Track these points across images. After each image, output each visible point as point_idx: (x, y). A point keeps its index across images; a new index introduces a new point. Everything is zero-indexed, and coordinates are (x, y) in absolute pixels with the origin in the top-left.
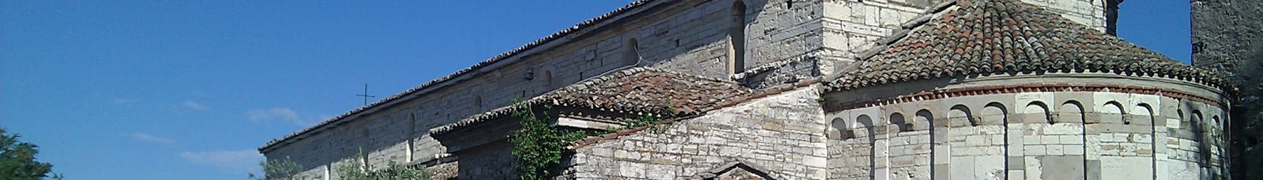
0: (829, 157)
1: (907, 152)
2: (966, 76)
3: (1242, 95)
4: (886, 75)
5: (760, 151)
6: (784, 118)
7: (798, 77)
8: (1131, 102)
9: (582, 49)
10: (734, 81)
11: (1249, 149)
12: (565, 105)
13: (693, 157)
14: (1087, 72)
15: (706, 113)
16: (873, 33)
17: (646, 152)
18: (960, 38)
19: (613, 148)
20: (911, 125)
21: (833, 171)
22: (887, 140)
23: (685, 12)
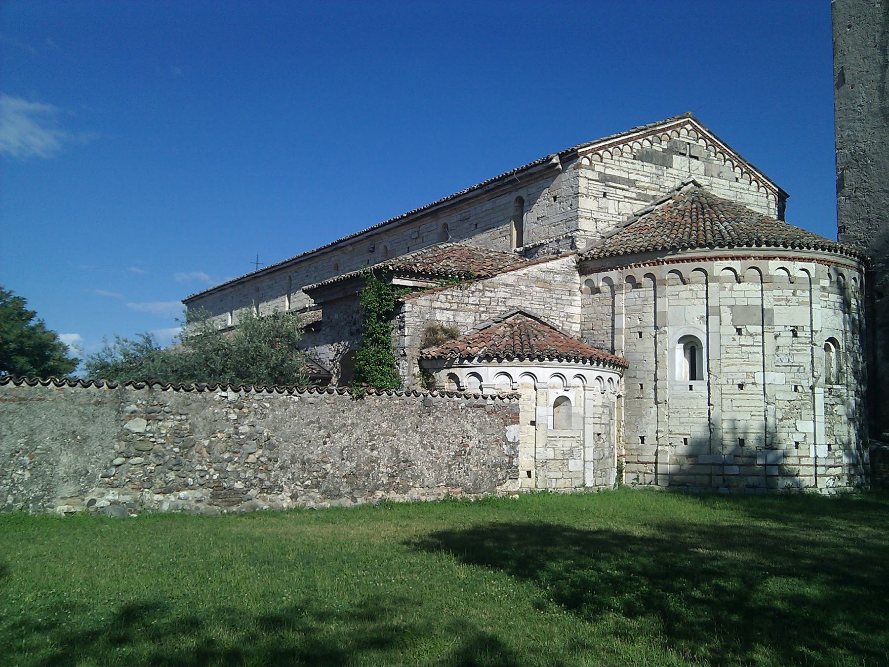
0: (583, 307)
1: (637, 303)
2: (679, 249)
4: (622, 249)
5: (534, 302)
6: (551, 279)
7: (561, 250)
8: (795, 268)
9: (409, 231)
11: (878, 301)
12: (397, 270)
13: (487, 306)
14: (764, 246)
15: (496, 275)
16: (614, 219)
19: (431, 300)
20: (640, 284)
23: (481, 205)
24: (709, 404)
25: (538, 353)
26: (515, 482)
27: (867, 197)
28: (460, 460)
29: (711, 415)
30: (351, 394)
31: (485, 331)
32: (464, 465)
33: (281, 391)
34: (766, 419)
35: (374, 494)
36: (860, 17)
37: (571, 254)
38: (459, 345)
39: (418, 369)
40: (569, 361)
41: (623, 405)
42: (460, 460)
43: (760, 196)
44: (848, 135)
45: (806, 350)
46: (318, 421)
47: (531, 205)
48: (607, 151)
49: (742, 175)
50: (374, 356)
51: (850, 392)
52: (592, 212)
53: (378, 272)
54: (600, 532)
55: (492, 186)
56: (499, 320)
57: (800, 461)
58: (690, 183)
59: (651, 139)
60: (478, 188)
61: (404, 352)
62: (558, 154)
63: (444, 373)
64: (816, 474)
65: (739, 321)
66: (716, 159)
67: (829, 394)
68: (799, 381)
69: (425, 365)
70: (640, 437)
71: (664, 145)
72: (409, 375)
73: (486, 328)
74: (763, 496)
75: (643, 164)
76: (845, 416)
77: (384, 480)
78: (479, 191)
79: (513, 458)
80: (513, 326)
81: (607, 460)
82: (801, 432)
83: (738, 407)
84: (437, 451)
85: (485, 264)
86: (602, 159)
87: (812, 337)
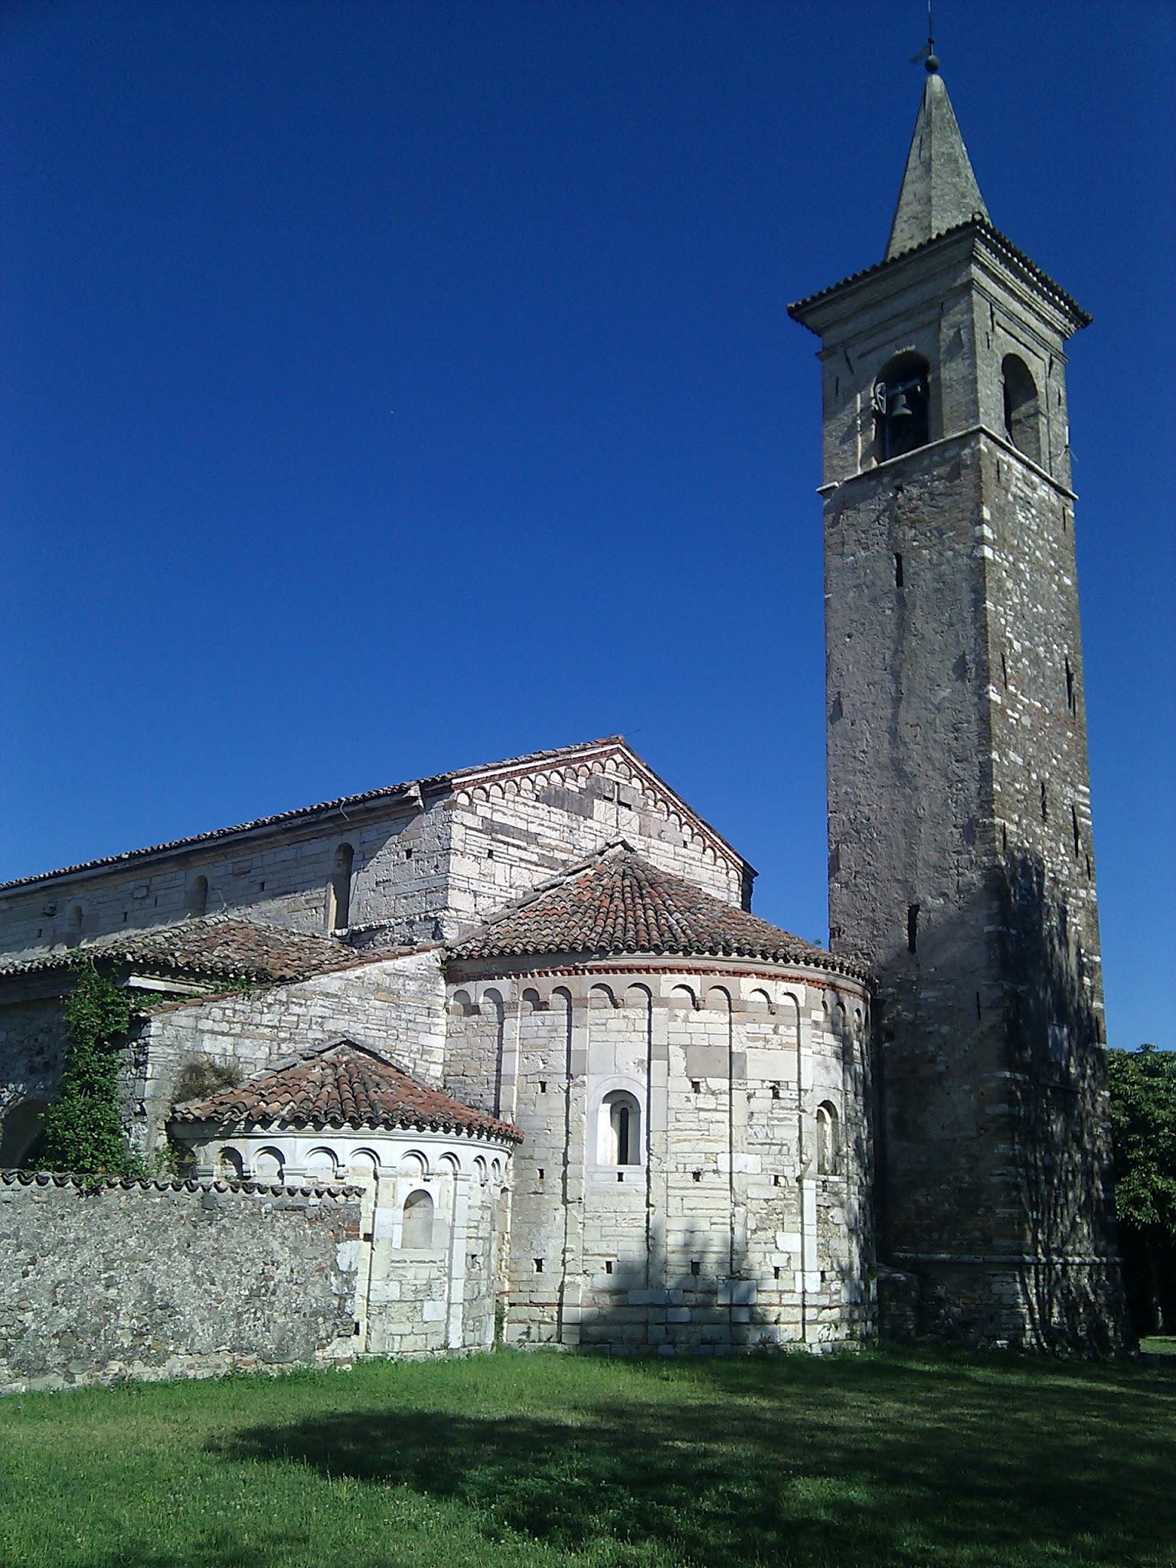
0: (449, 1035)
1: (540, 1034)
2: (609, 952)
3: (880, 988)
4: (520, 945)
5: (370, 1026)
6: (400, 987)
7: (415, 939)
8: (778, 990)
9: (129, 884)
10: (334, 938)
11: (887, 1045)
12: (141, 961)
13: (292, 1030)
14: (734, 955)
15: (310, 978)
16: (503, 894)
17: (236, 1023)
18: (600, 907)
19: (196, 1017)
20: (546, 1003)
21: (451, 1052)
22: (519, 1019)
23: (273, 850)
24: (648, 1205)
25: (385, 1115)
26: (346, 1343)
27: (872, 887)
28: (258, 1304)
29: (651, 1222)
30: (78, 1185)
31: (286, 1074)
32: (263, 1313)
33: (28, 1181)
34: (732, 1229)
35: (106, 1366)
36: (864, 624)
37: (434, 948)
38: (244, 1098)
39: (165, 1139)
40: (434, 1129)
41: (510, 1205)
42: (258, 1304)
43: (717, 871)
44: (846, 793)
45: (791, 1120)
46: (16, 1234)
47: (366, 860)
48: (497, 784)
49: (693, 837)
50: (83, 1113)
51: (852, 1187)
52: (470, 880)
53: (104, 963)
54: (509, 1421)
55: (299, 821)
56: (312, 1054)
57: (781, 1298)
58: (617, 844)
59: (563, 772)
60: (271, 823)
61: (142, 1108)
62: (418, 782)
63: (215, 1147)
64: (804, 1319)
65: (695, 1071)
66: (656, 810)
67: (824, 1191)
68: (780, 1168)
69: (178, 1131)
70: (536, 1260)
71: (582, 782)
72: (147, 1149)
73: (288, 1068)
74: (729, 1357)
75: (549, 809)
76: (845, 1226)
77: (124, 1340)
78: (274, 828)
79: (346, 1300)
80: (336, 1066)
81: (484, 1302)
82: (782, 1252)
83: (692, 1209)
84: (220, 1289)
85: (287, 956)
86: (488, 796)
87: (800, 1100)
